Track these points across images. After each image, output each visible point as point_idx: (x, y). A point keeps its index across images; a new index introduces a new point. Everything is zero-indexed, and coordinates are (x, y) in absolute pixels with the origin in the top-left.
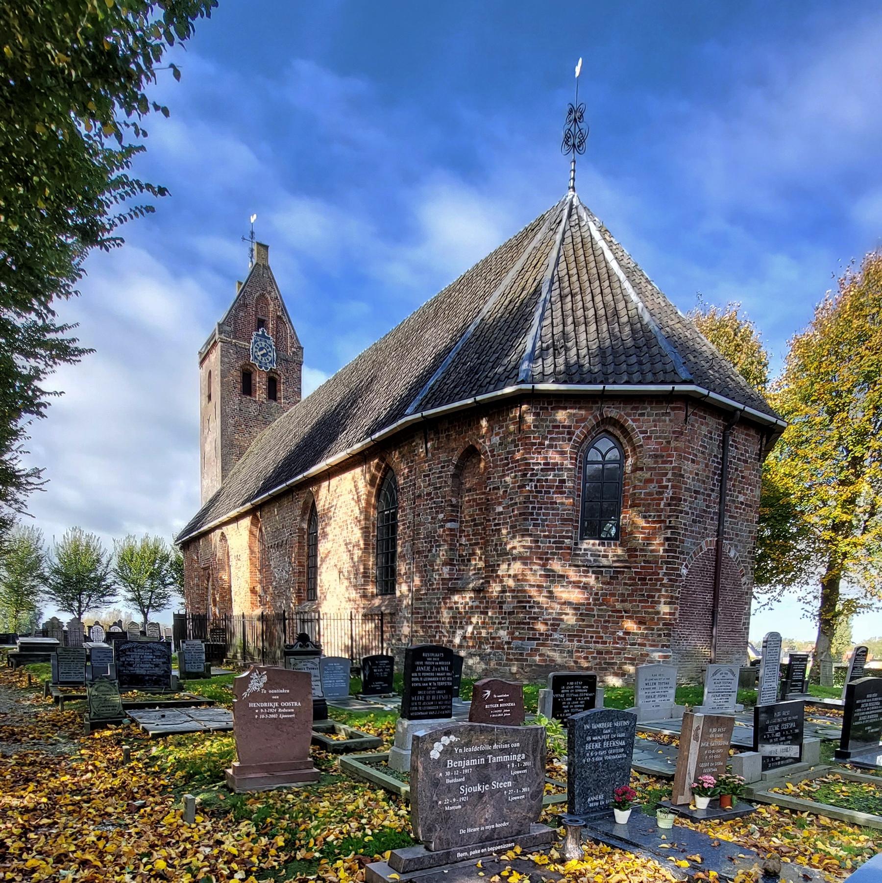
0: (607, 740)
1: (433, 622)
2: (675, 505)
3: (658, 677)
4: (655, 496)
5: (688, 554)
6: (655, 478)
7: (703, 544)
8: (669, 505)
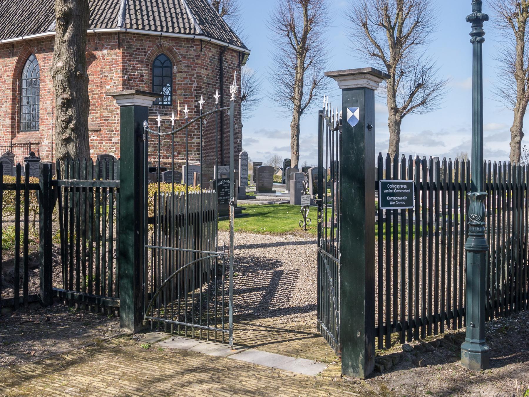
2: (199, 90)
6: (188, 77)
8: (196, 90)
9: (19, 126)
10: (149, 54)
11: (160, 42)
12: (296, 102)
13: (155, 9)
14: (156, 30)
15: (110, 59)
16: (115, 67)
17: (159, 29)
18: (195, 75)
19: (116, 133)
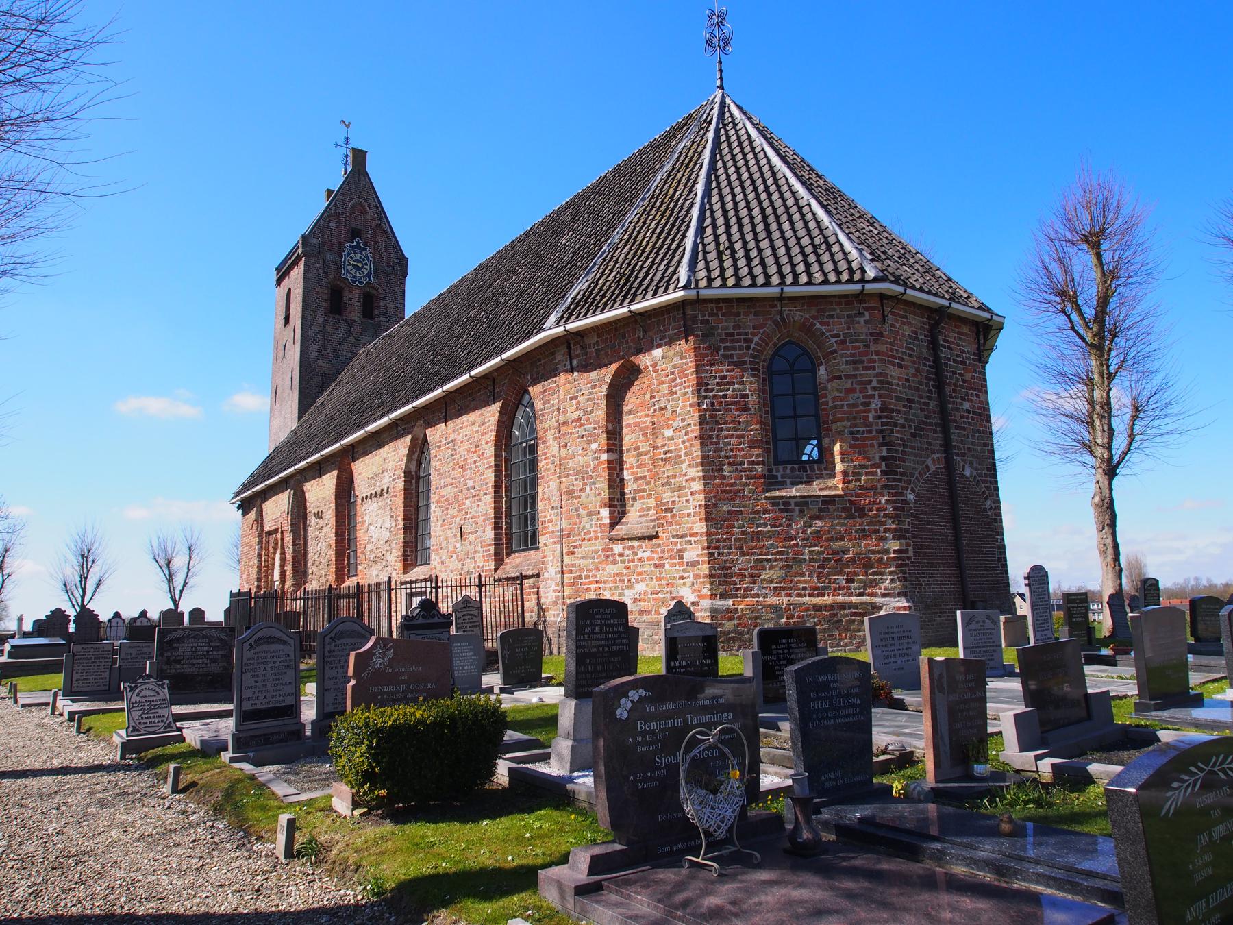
0: (837, 696)
1: (591, 583)
2: (887, 417)
3: (895, 630)
4: (861, 408)
5: (912, 474)
6: (858, 387)
7: (929, 462)
8: (879, 417)
9: (509, 541)
10: (757, 343)
11: (781, 313)
12: (1099, 451)
13: (765, 244)
14: (767, 284)
15: (668, 367)
16: (681, 384)
17: (775, 280)
18: (875, 380)
19: (692, 539)
